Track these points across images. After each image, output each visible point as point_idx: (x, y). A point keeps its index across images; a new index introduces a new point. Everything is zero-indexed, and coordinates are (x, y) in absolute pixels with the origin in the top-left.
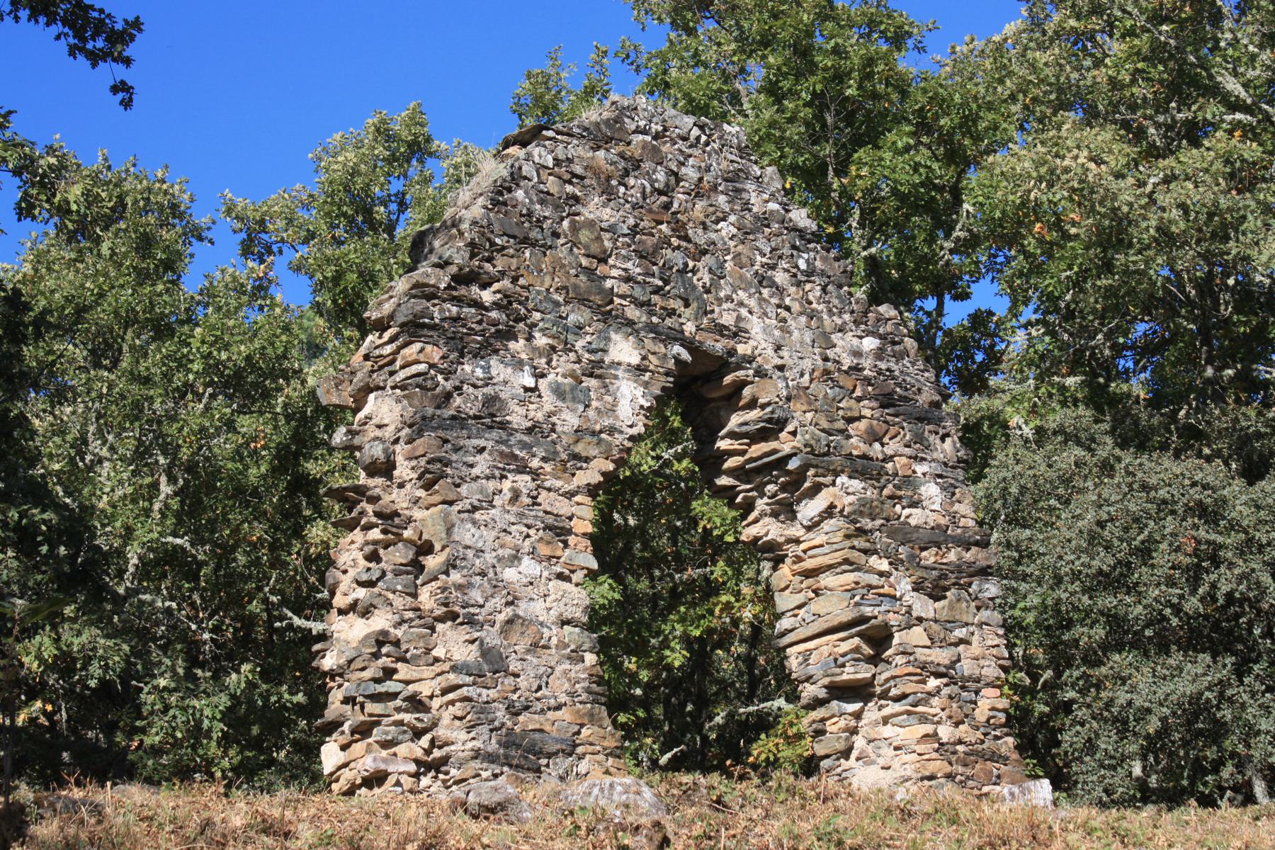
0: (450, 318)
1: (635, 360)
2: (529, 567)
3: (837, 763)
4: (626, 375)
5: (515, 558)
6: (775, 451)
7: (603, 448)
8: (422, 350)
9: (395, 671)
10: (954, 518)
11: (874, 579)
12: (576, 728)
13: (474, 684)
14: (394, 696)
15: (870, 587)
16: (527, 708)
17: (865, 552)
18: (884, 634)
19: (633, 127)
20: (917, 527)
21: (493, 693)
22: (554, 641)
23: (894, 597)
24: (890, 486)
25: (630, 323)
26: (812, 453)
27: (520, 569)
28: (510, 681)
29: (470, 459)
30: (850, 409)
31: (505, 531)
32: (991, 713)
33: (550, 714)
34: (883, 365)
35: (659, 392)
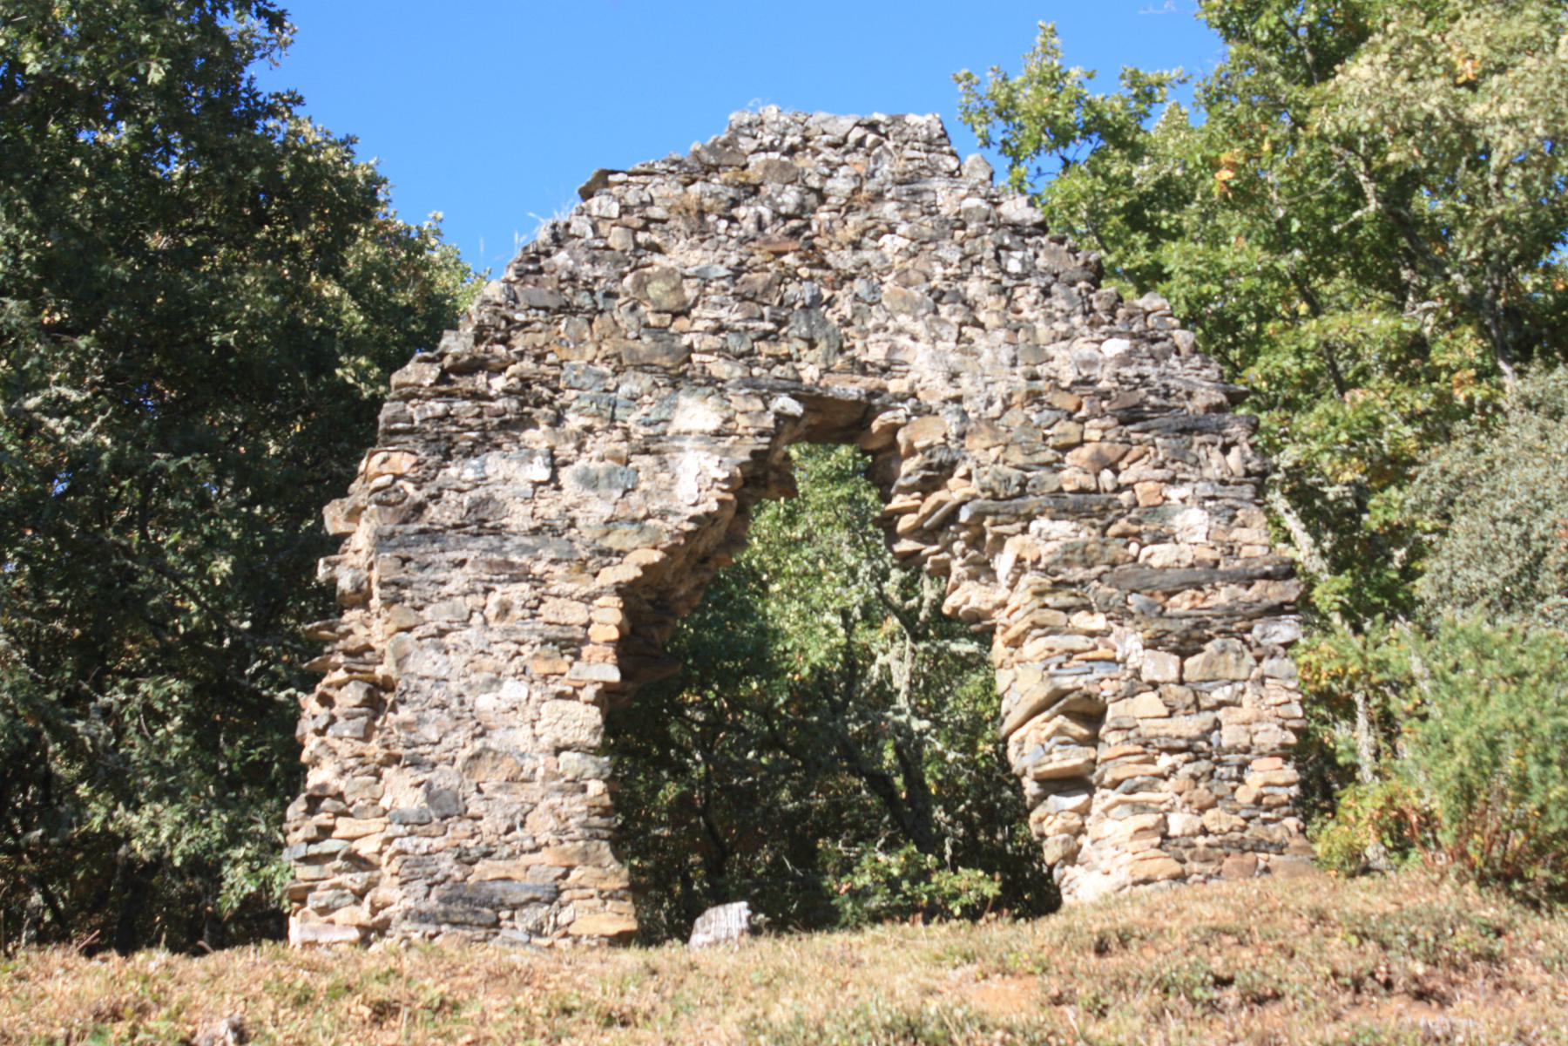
1: (714, 423)
2: (514, 690)
5: (496, 681)
6: (940, 504)
7: (647, 536)
8: (385, 461)
9: (333, 828)
11: (1079, 642)
12: (560, 871)
13: (410, 834)
14: (332, 856)
16: (487, 855)
17: (1066, 610)
18: (1094, 709)
19: (754, 145)
20: (1164, 568)
21: (438, 843)
22: (540, 772)
23: (1113, 660)
24: (1123, 522)
25: (711, 381)
26: (995, 497)
28: (467, 825)
29: (441, 576)
30: (1065, 435)
33: (526, 859)
34: (1129, 372)
35: (747, 458)
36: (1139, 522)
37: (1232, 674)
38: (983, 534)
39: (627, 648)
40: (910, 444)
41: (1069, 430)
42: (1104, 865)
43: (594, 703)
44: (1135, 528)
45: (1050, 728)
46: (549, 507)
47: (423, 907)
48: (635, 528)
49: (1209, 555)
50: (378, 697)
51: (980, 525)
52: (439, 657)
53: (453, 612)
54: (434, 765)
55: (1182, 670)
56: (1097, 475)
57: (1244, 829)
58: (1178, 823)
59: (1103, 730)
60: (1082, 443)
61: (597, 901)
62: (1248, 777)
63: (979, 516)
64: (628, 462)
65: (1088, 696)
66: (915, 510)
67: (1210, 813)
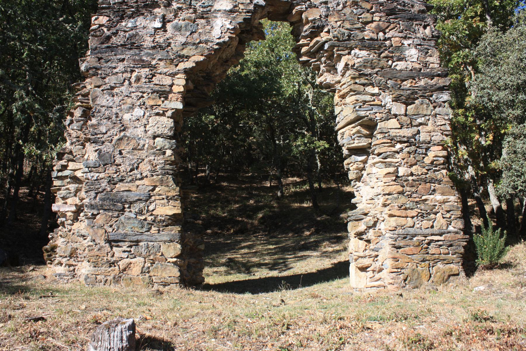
0: (118, 3)
2: (138, 112)
3: (355, 183)
4: (222, 15)
5: (132, 107)
6: (317, 42)
9: (67, 166)
10: (426, 65)
11: (368, 98)
12: (151, 188)
13: (90, 172)
14: (66, 177)
15: (365, 102)
16: (122, 181)
17: (364, 85)
18: (373, 124)
20: (401, 70)
21: (102, 175)
23: (381, 105)
24: (386, 52)
26: (338, 40)
27: (133, 114)
29: (114, 65)
30: (366, 18)
31: (127, 96)
32: (435, 158)
33: (138, 182)
36: (392, 52)
37: (425, 113)
38: (333, 54)
39: (187, 97)
40: (307, 18)
41: (367, 16)
42: (372, 184)
43: (171, 118)
44: (391, 55)
45: (354, 130)
46: (160, 39)
47: (93, 202)
48: (194, 47)
49: (418, 66)
50: (87, 114)
51: (332, 51)
52: (110, 98)
53: (117, 80)
54: (103, 143)
55: (406, 110)
56: (377, 34)
57: (427, 174)
58: (402, 171)
59: (375, 133)
60: (372, 21)
61: (166, 201)
62: (429, 154)
63: (332, 47)
64: (195, 21)
65: (371, 119)
66: (307, 45)
67: (414, 167)
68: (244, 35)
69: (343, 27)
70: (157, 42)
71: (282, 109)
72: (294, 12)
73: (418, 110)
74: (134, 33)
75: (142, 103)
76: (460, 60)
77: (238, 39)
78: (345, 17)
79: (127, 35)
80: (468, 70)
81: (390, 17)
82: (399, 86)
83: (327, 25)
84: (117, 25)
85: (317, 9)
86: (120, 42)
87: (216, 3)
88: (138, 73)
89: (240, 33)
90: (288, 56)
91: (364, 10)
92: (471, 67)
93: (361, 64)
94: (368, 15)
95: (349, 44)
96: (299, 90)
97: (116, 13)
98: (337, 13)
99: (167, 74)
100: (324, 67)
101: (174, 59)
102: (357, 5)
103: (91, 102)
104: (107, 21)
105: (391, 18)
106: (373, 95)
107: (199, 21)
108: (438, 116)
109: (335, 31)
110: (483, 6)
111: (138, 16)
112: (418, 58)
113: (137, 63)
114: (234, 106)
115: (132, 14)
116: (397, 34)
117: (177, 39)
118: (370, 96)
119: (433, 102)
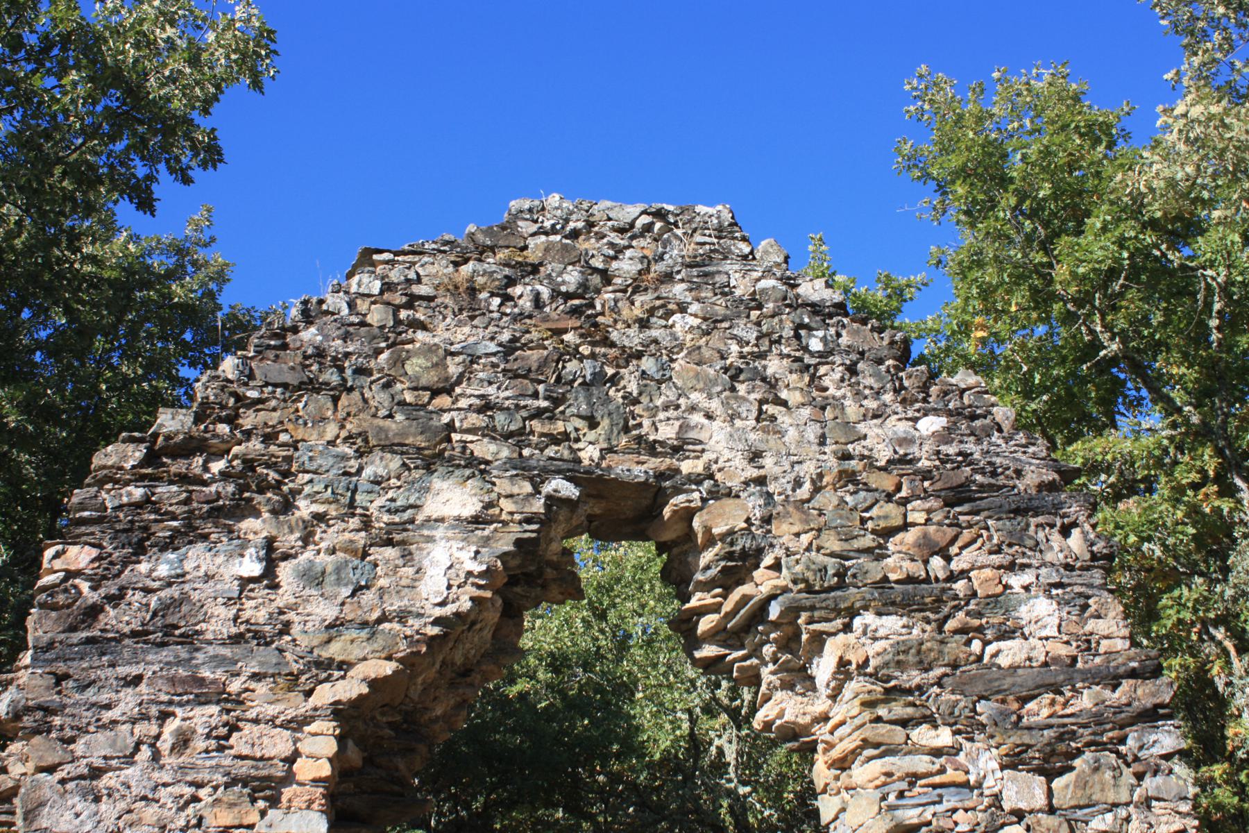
0: (129, 505)
4: (450, 534)
6: (745, 599)
10: (1088, 645)
11: (922, 763)
15: (913, 778)
17: (904, 723)
20: (1014, 668)
23: (966, 785)
24: (961, 615)
26: (809, 590)
29: (104, 697)
30: (886, 517)
31: (144, 798)
34: (951, 450)
36: (980, 615)
37: (1111, 797)
38: (798, 634)
40: (707, 530)
41: (888, 512)
44: (976, 622)
46: (257, 611)
48: (364, 634)
53: (113, 744)
55: (1050, 794)
56: (926, 562)
60: (905, 526)
63: (792, 612)
64: (365, 554)
66: (716, 608)
68: (518, 589)
69: (819, 549)
70: (247, 622)
71: (638, 794)
72: (667, 512)
73: (1088, 792)
74: (176, 595)
75: (194, 821)
76: (1187, 616)
77: (499, 602)
78: (822, 519)
79: (154, 601)
80: (1212, 638)
81: (958, 509)
82: (1014, 718)
83: (772, 546)
84: (121, 572)
85: (737, 501)
86: (128, 623)
87: (429, 496)
88: (184, 720)
89: (505, 584)
90: (651, 630)
91: (877, 495)
92: (1222, 630)
93: (888, 657)
94: (891, 508)
95: (844, 599)
96: (692, 734)
97: (123, 537)
98: (797, 508)
99: (278, 722)
100: (773, 673)
101: (302, 673)
102: (856, 483)
103: (20, 822)
104: (93, 561)
105: (960, 513)
106: (937, 752)
107: (378, 553)
108: (1154, 803)
109: (797, 562)
110: (1219, 452)
111: (190, 542)
112: (1060, 626)
113: (180, 690)
114: (488, 795)
115: (171, 537)
116: (984, 558)
117: (309, 609)
118: (927, 758)
119: (1130, 759)
